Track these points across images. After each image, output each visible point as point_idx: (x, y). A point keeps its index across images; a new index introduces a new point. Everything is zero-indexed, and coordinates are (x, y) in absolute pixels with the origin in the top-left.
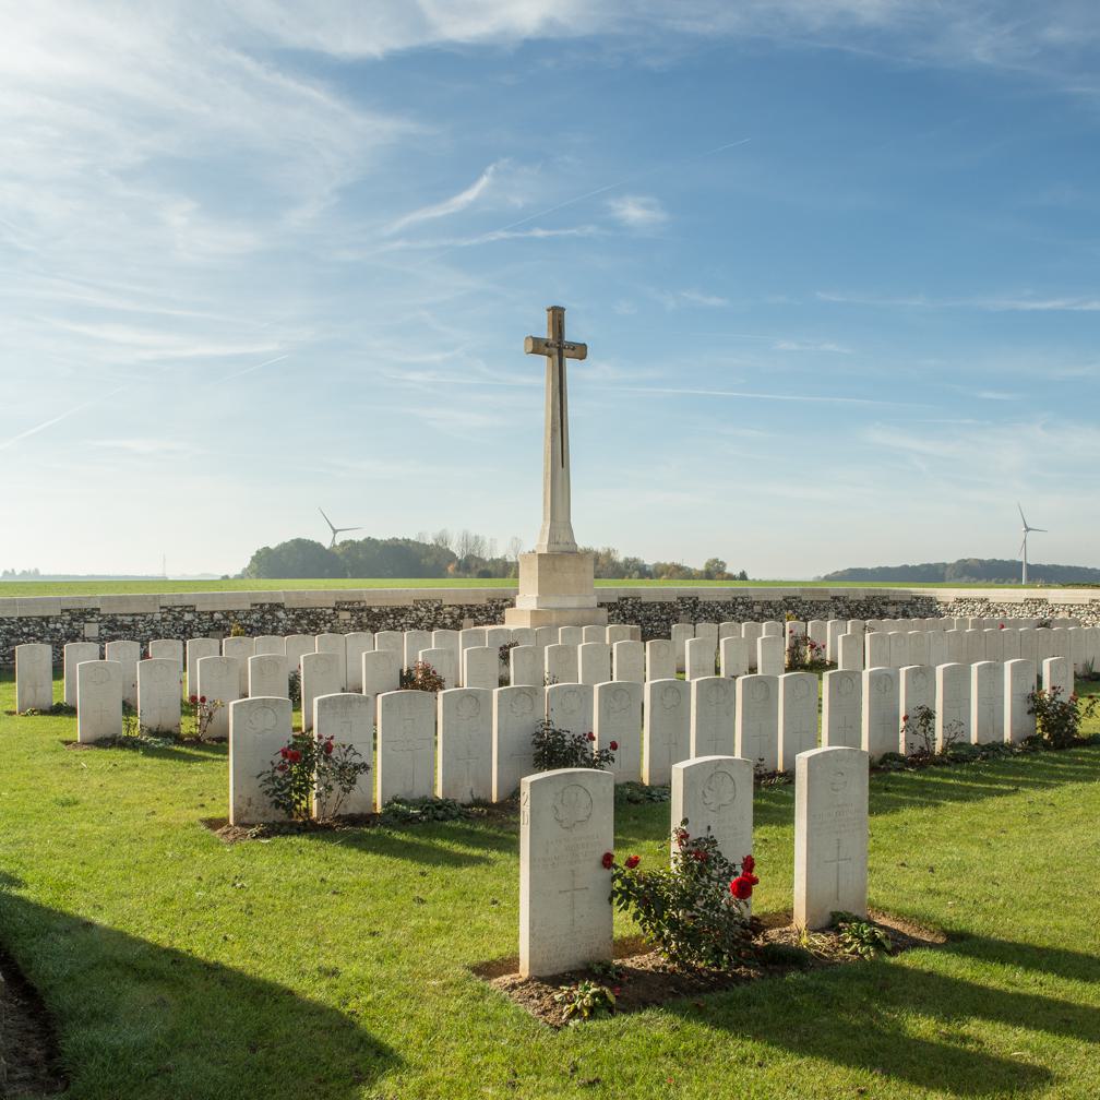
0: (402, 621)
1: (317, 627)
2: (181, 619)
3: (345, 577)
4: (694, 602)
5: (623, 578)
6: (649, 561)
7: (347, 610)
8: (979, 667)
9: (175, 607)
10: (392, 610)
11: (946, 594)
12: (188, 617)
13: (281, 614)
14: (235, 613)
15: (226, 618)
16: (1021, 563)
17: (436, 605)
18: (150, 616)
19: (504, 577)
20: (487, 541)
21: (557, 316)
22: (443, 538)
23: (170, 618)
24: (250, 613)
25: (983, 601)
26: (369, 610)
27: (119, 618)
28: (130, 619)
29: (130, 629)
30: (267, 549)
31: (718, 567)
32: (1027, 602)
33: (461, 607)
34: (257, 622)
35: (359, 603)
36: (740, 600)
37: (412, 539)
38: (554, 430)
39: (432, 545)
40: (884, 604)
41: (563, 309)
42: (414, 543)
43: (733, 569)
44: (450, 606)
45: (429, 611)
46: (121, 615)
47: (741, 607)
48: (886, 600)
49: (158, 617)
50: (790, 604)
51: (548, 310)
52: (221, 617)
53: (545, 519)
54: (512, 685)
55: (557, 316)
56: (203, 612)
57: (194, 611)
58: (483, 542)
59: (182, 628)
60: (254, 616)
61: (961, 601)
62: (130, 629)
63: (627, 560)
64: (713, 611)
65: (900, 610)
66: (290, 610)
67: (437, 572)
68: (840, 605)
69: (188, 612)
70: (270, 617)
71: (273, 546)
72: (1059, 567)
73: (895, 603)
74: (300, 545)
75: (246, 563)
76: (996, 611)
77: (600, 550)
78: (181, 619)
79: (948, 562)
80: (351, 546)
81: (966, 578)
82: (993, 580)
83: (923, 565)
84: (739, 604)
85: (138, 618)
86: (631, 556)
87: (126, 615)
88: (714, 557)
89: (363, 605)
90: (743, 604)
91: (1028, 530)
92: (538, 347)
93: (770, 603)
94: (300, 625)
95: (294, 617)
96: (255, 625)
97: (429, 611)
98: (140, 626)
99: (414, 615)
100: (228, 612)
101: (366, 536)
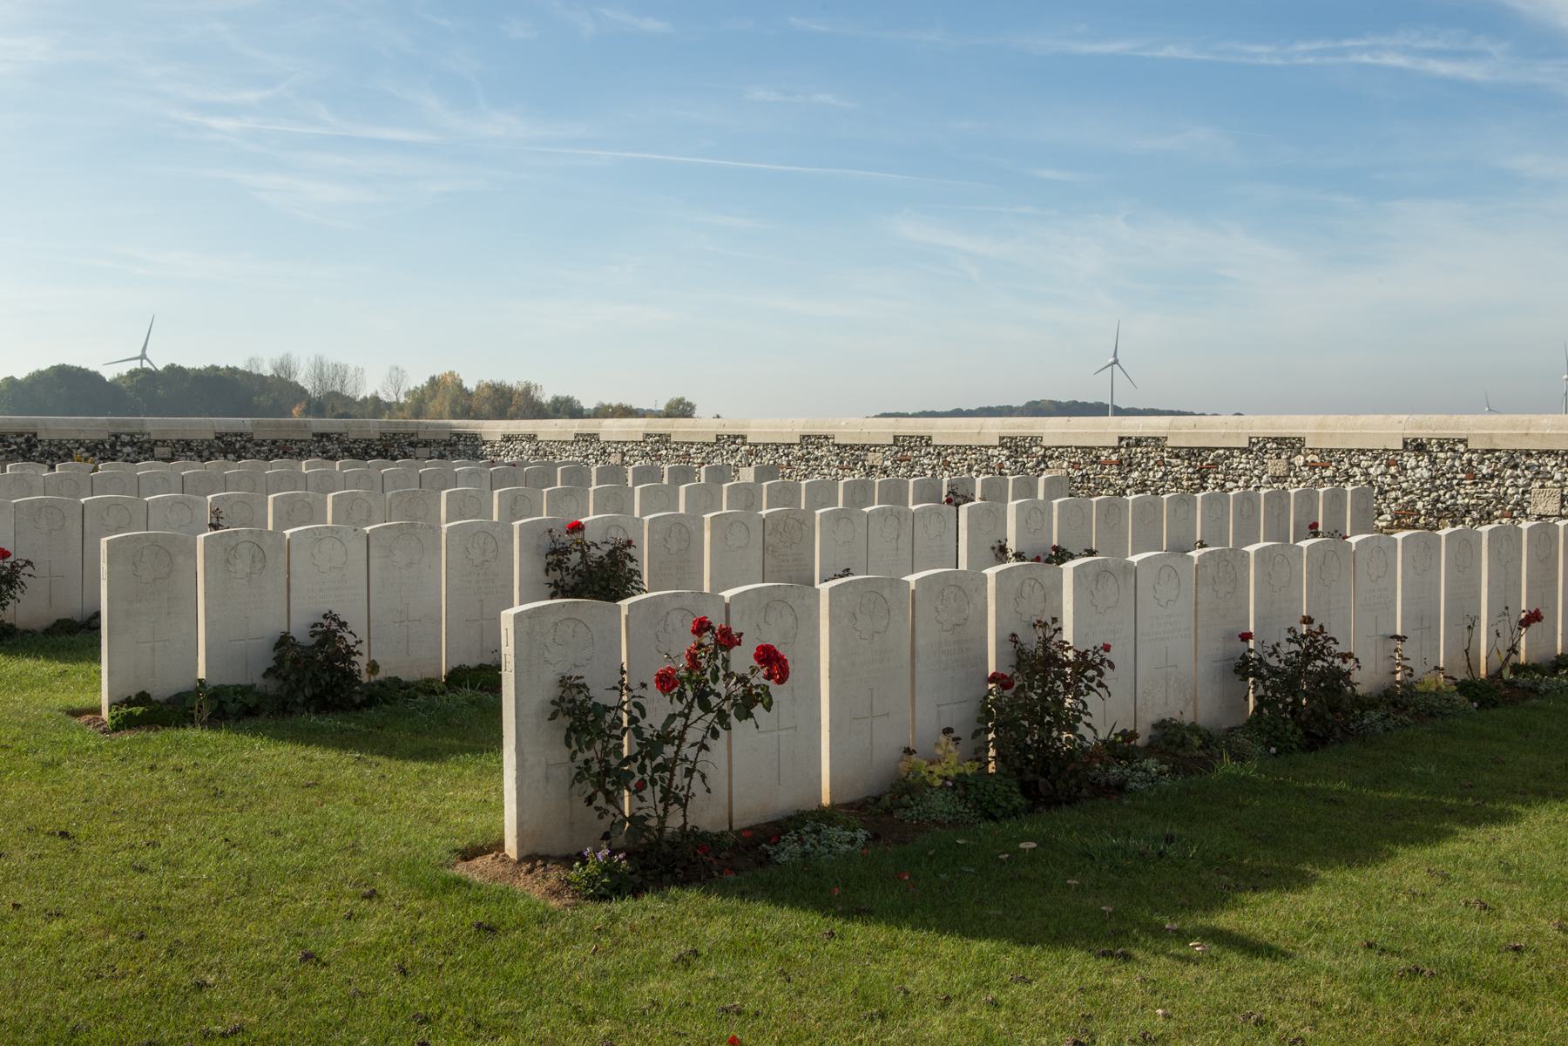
4: (28, 440)
8: (641, 489)
11: (493, 429)
20: (351, 371)
22: (285, 366)
36: (126, 438)
37: (241, 366)
40: (411, 444)
42: (244, 373)
50: (232, 444)
54: (978, 501)
56: (946, 447)
71: (20, 375)
74: (64, 375)
79: (1014, 405)
83: (1097, 403)
84: (124, 444)
88: (679, 396)
90: (132, 444)
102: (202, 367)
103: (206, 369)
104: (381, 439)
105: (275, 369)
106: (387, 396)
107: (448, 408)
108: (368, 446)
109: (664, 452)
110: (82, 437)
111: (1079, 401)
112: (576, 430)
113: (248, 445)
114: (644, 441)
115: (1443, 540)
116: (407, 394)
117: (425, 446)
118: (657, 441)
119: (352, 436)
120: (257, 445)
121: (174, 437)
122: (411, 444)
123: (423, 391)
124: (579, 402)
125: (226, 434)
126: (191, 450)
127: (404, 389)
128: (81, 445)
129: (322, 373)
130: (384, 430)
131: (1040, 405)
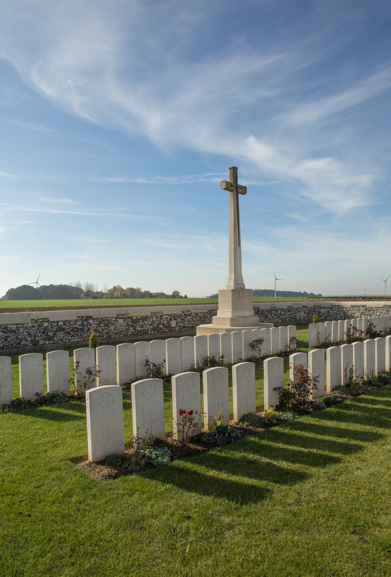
0: (146, 323)
1: (108, 327)
2: (42, 326)
3: (42, 299)
4: (258, 310)
5: (144, 298)
7: (122, 318)
9: (39, 319)
10: (142, 318)
12: (46, 324)
13: (91, 321)
14: (69, 322)
15: (65, 324)
16: (275, 290)
17: (160, 315)
18: (26, 325)
19: (102, 298)
20: (95, 286)
23: (36, 325)
24: (76, 321)
25: (363, 306)
26: (132, 318)
27: (9, 326)
28: (15, 326)
29: (15, 332)
30: (12, 289)
31: (177, 294)
32: (384, 306)
33: (170, 315)
34: (80, 326)
35: (127, 314)
36: (273, 308)
37: (68, 285)
38: (235, 228)
39: (75, 287)
40: (320, 308)
41: (237, 168)
43: (182, 294)
44: (166, 315)
45: (157, 317)
46: (10, 325)
47: (274, 311)
48: (321, 307)
49: (30, 325)
50: (289, 309)
51: (230, 169)
52: (62, 324)
53: (230, 272)
56: (53, 322)
57: (49, 321)
58: (94, 286)
59: (43, 330)
60: (79, 323)
61: (353, 306)
62: (15, 332)
63: (145, 291)
64: (264, 313)
65: (326, 311)
66: (95, 319)
67: (77, 297)
68: (305, 309)
69: (46, 322)
70: (86, 323)
71: (15, 288)
72: (285, 291)
73: (324, 308)
74: (25, 287)
75: (4, 294)
76: (370, 310)
77: (136, 288)
78: (42, 326)
80: (44, 288)
81: (256, 296)
82: (265, 296)
84: (273, 310)
85: (19, 326)
86: (146, 290)
87: (13, 325)
88: (176, 290)
89: (129, 315)
90: (274, 310)
91: (276, 279)
93: (283, 309)
94: (100, 327)
95: (97, 322)
96: (79, 327)
97: (157, 317)
98: (21, 330)
99: (151, 320)
100: (66, 321)
101: (50, 284)
103: (59, 285)
105: (76, 285)
106: (104, 291)
107: (119, 294)
111: (266, 289)
112: (383, 304)
115: (232, 334)
116: (108, 291)
117: (324, 308)
121: (281, 308)
122: (320, 308)
123: (112, 290)
127: (107, 290)
129: (88, 286)
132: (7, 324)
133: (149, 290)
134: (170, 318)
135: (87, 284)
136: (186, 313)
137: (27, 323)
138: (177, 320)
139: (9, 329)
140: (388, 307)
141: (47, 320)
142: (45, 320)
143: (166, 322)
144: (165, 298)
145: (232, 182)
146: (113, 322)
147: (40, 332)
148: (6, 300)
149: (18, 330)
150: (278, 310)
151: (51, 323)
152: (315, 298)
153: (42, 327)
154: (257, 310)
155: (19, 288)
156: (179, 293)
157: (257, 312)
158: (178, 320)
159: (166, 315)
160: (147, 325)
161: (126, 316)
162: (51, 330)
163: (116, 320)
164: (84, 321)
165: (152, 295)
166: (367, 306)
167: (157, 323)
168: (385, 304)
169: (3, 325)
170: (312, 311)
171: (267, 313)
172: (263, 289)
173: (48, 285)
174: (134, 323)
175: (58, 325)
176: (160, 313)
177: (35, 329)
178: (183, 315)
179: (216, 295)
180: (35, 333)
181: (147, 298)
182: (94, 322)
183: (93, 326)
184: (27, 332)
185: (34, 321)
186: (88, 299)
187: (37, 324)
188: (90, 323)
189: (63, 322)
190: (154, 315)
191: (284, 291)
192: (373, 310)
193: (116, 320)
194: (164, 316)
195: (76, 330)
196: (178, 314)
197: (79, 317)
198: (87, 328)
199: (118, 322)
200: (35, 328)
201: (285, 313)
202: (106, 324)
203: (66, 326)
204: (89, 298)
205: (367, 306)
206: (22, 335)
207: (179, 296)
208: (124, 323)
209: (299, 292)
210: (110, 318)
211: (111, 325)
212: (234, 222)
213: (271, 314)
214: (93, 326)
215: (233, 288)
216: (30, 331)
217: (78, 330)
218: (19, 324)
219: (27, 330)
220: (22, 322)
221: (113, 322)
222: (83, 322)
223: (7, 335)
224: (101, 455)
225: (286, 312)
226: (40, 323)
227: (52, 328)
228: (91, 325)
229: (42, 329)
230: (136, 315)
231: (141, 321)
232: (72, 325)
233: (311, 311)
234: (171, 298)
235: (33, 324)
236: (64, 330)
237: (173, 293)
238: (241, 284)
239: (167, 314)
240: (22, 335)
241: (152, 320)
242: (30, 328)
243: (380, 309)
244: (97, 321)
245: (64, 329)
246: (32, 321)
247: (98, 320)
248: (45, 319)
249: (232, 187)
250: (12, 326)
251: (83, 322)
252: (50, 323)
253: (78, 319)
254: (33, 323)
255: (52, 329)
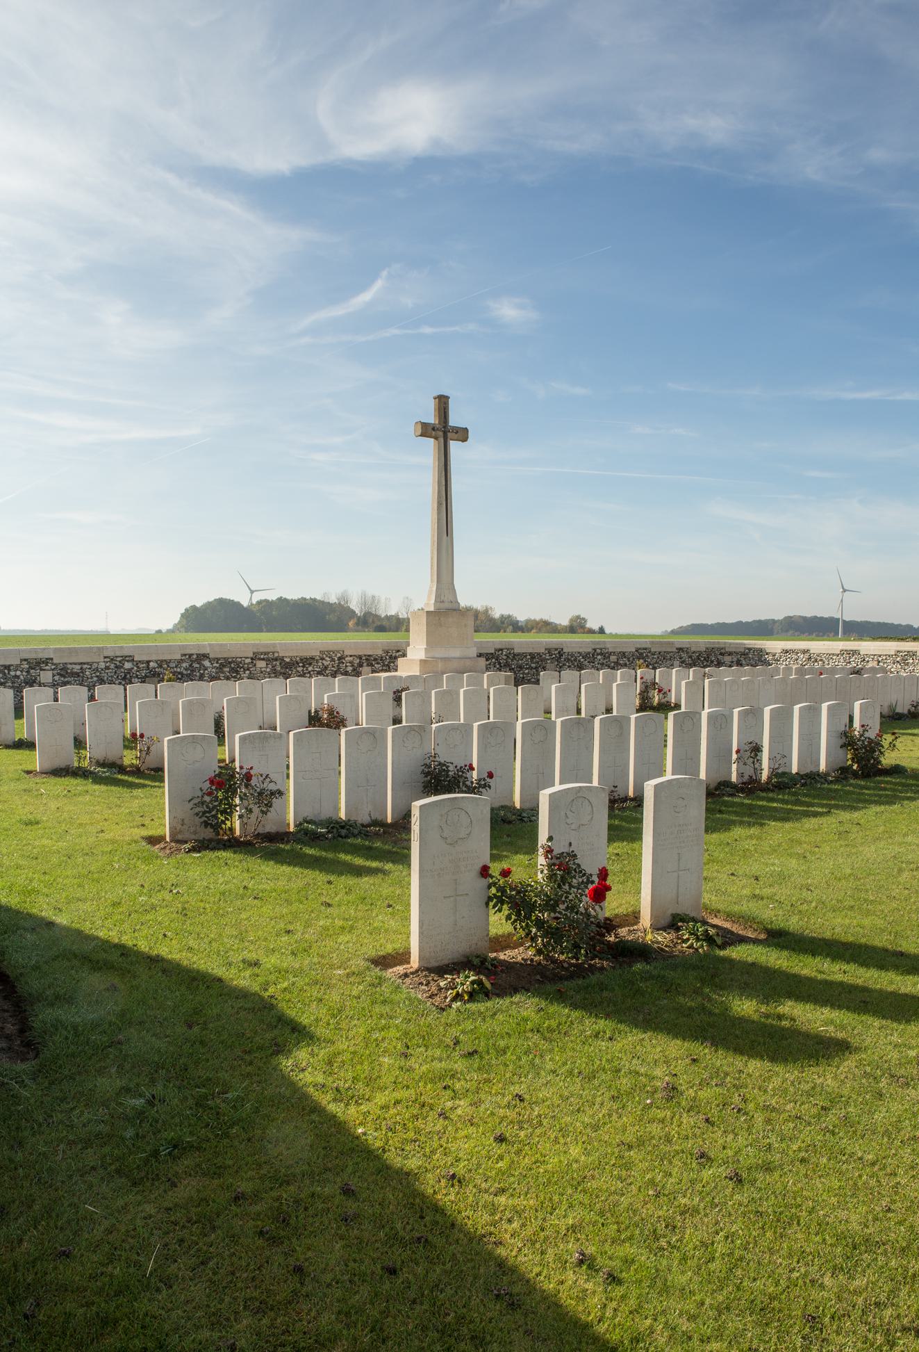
0: (310, 669)
1: (237, 674)
2: (122, 667)
4: (559, 652)
6: (521, 617)
7: (263, 659)
9: (117, 657)
10: (301, 660)
12: (128, 665)
13: (207, 663)
14: (168, 662)
15: (160, 666)
17: (339, 655)
20: (383, 600)
21: (443, 403)
22: (344, 597)
23: (112, 666)
24: (181, 661)
25: (805, 652)
26: (282, 659)
27: (69, 666)
28: (79, 667)
29: (79, 676)
30: (194, 607)
32: (842, 652)
33: (360, 657)
35: (273, 653)
36: (598, 651)
37: (319, 598)
38: (439, 504)
40: (721, 654)
41: (447, 398)
43: (593, 624)
44: (351, 656)
45: (333, 660)
47: (599, 657)
49: (102, 665)
50: (642, 654)
51: (435, 398)
52: (156, 665)
53: (432, 581)
55: (443, 403)
56: (140, 661)
60: (184, 665)
61: (787, 652)
62: (79, 676)
64: (575, 660)
65: (735, 659)
66: (214, 659)
67: (340, 627)
69: (128, 661)
70: (198, 666)
71: (199, 605)
72: (870, 623)
73: (730, 654)
74: (222, 603)
75: (177, 619)
76: (816, 661)
78: (122, 667)
81: (791, 632)
84: (598, 655)
85: (85, 666)
86: (506, 613)
87: (75, 664)
89: (276, 655)
90: (601, 654)
91: (845, 591)
92: (426, 430)
93: (624, 653)
94: (223, 673)
95: (218, 665)
96: (185, 672)
97: (333, 660)
98: (87, 673)
99: (320, 664)
100: (162, 661)
101: (279, 596)
102: (296, 598)
104: (706, 651)
105: (338, 599)
108: (700, 654)
109: (911, 661)
110: (581, 650)
112: (841, 648)
113: (649, 654)
114: (895, 655)
117: (729, 655)
118: (906, 655)
119: (693, 649)
120: (652, 654)
121: (619, 650)
124: (516, 618)
125: (640, 649)
126: (625, 657)
127: (411, 610)
128: (580, 655)
130: (708, 646)
131: (793, 619)
132: (66, 663)
133: (511, 614)
134: (360, 662)
135: (363, 597)
136: (394, 655)
137: (98, 663)
138: (373, 666)
139: (69, 671)
140: (850, 654)
141: (131, 659)
142: (127, 659)
143: (351, 668)
144: (551, 632)
145: (437, 422)
146: (246, 666)
147: (118, 677)
148: (180, 632)
149: (83, 673)
150: (610, 654)
151: (137, 664)
152: (891, 638)
153: (123, 670)
154: (556, 652)
155: (209, 605)
156: (585, 621)
157: (556, 657)
158: (376, 665)
159: (351, 656)
160: (312, 673)
161: (270, 656)
162: (137, 676)
163: (252, 662)
164: (194, 661)
165: (520, 624)
166: (811, 652)
167: (332, 670)
168: (845, 648)
169: (60, 664)
170: (702, 659)
171: (582, 660)
172: (809, 615)
173: (274, 599)
174: (287, 668)
175: (148, 667)
176: (338, 652)
177: (111, 672)
178: (387, 657)
179: (685, 627)
180: (110, 678)
181: (505, 632)
182: (212, 664)
183: (209, 670)
184: (97, 676)
185: (109, 660)
186: (365, 631)
187: (113, 665)
188: (204, 666)
189: (157, 662)
190: (327, 656)
191: (867, 621)
192: (821, 660)
193: (252, 662)
194: (346, 659)
195: (180, 676)
196: (377, 655)
197: (185, 655)
198: (198, 674)
199: (255, 665)
200: (111, 670)
201: (629, 661)
202: (233, 668)
203: (162, 670)
204: (367, 630)
205: (811, 652)
206: (90, 680)
207: (586, 630)
208: (267, 668)
209: (786, 618)
210: (241, 658)
211: (242, 670)
212: (439, 492)
213: (593, 663)
214: (209, 670)
215: (432, 609)
216: (103, 675)
217: (182, 676)
218: (84, 664)
219: (98, 674)
220: (89, 660)
221: (246, 666)
222: (192, 664)
223: (66, 679)
224: (48, 766)
225: (631, 659)
226: (118, 664)
227: (138, 671)
228: (206, 669)
229: (122, 672)
230: (291, 655)
231: (301, 665)
232: (173, 668)
233: (699, 659)
234: (565, 632)
235: (107, 665)
236: (159, 676)
237: (571, 620)
238: (449, 602)
239: (353, 654)
240: (90, 680)
241: (323, 664)
242: (102, 670)
243: (834, 657)
244: (217, 663)
245: (159, 675)
246: (106, 660)
247: (219, 662)
248: (126, 657)
249: (434, 433)
250: (74, 666)
251: (192, 664)
252: (135, 663)
253: (183, 658)
254: (107, 662)
255: (138, 673)
